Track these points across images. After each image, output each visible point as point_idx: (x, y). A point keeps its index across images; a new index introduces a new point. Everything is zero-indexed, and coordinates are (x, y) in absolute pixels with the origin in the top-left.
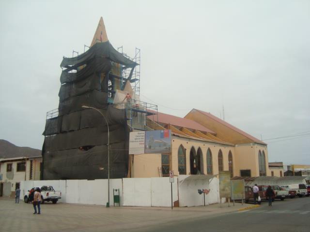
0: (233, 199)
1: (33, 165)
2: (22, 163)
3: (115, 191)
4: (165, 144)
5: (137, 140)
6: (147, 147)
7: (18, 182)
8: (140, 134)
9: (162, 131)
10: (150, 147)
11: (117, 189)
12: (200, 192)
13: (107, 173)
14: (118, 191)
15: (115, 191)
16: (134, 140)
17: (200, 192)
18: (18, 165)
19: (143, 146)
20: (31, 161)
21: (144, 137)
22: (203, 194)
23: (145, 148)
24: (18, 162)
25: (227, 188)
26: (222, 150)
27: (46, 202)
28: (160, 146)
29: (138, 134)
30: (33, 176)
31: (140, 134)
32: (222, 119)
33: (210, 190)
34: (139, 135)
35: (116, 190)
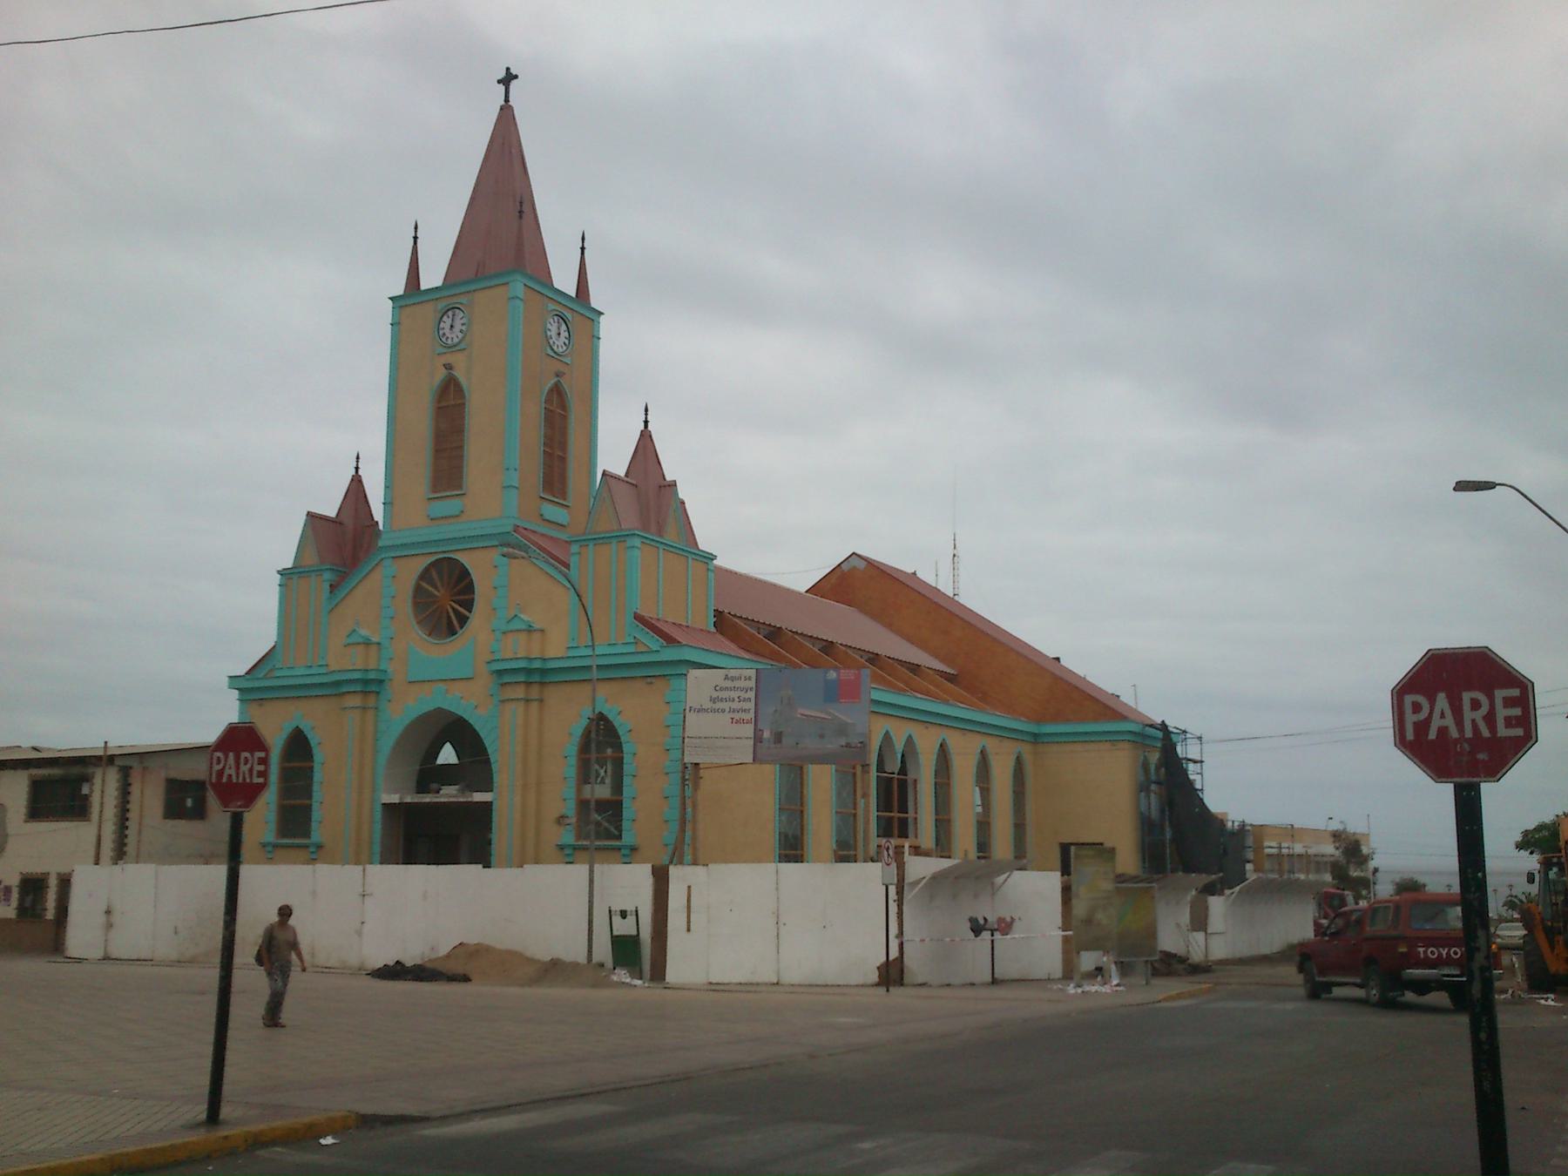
0: (362, 890)
1: (135, 790)
2: (64, 781)
3: (617, 919)
4: (842, 729)
5: (719, 705)
6: (766, 735)
7: (64, 870)
8: (733, 679)
9: (832, 675)
10: (778, 737)
11: (630, 908)
12: (977, 929)
13: (1453, 981)
14: (631, 919)
15: (617, 919)
16: (708, 705)
17: (977, 929)
18: (37, 787)
19: (749, 730)
20: (125, 772)
21: (752, 695)
22: (986, 935)
23: (758, 739)
24: (35, 772)
25: (1100, 916)
26: (989, 750)
27: (1410, 996)
28: (822, 736)
29: (726, 678)
30: (131, 840)
31: (733, 679)
32: (1134, 707)
33: (1013, 920)
34: (729, 684)
35: (624, 914)
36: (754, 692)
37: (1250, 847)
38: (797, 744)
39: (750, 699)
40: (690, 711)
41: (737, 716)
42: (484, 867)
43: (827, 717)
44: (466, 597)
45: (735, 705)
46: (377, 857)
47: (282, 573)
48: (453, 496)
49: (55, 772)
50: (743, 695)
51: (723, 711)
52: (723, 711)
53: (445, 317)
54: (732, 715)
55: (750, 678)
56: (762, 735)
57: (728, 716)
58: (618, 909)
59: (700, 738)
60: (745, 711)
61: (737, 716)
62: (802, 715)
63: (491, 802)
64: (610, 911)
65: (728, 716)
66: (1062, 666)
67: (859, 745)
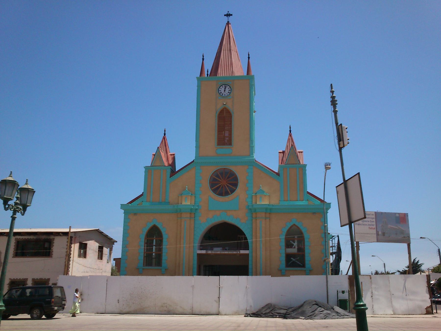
3: (340, 294)
6: (380, 233)
10: (384, 234)
19: (374, 231)
23: (378, 234)
28: (396, 234)
36: (375, 219)
37: (155, 308)
38: (389, 236)
39: (374, 221)
40: (356, 224)
41: (371, 227)
42: (272, 277)
43: (397, 228)
44: (216, 178)
45: (370, 223)
46: (196, 273)
47: (146, 168)
48: (302, 158)
49: (32, 237)
50: (372, 220)
51: (366, 225)
52: (366, 225)
53: (221, 87)
54: (369, 226)
55: (373, 215)
56: (379, 233)
57: (368, 227)
58: (341, 290)
59: (360, 233)
60: (373, 225)
61: (371, 227)
62: (390, 227)
63: (249, 254)
64: (337, 291)
65: (368, 227)
66: (144, 191)
67: (407, 237)
